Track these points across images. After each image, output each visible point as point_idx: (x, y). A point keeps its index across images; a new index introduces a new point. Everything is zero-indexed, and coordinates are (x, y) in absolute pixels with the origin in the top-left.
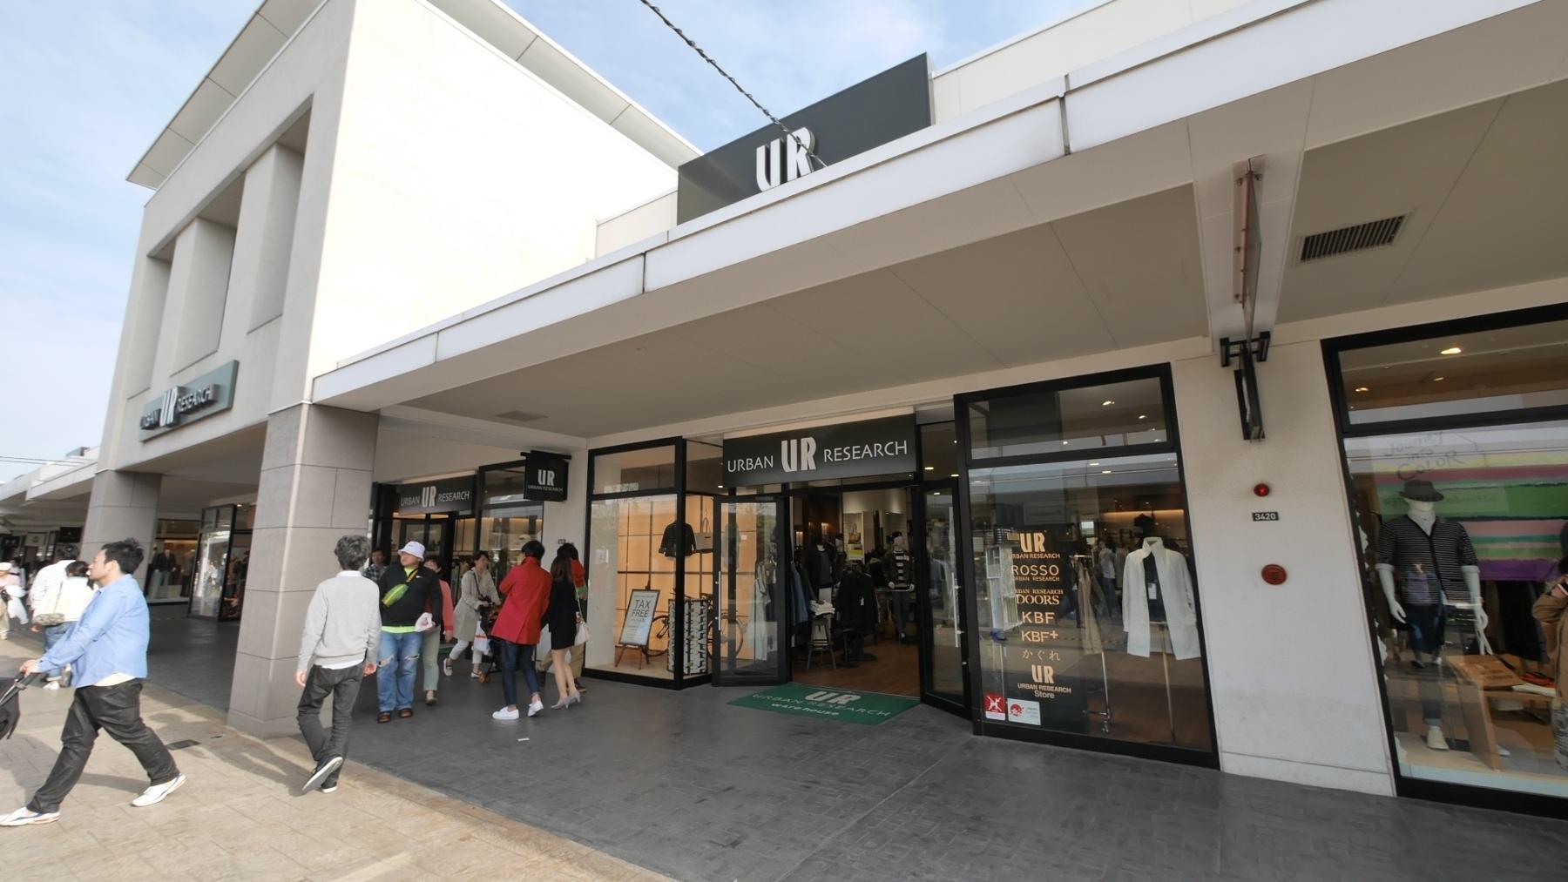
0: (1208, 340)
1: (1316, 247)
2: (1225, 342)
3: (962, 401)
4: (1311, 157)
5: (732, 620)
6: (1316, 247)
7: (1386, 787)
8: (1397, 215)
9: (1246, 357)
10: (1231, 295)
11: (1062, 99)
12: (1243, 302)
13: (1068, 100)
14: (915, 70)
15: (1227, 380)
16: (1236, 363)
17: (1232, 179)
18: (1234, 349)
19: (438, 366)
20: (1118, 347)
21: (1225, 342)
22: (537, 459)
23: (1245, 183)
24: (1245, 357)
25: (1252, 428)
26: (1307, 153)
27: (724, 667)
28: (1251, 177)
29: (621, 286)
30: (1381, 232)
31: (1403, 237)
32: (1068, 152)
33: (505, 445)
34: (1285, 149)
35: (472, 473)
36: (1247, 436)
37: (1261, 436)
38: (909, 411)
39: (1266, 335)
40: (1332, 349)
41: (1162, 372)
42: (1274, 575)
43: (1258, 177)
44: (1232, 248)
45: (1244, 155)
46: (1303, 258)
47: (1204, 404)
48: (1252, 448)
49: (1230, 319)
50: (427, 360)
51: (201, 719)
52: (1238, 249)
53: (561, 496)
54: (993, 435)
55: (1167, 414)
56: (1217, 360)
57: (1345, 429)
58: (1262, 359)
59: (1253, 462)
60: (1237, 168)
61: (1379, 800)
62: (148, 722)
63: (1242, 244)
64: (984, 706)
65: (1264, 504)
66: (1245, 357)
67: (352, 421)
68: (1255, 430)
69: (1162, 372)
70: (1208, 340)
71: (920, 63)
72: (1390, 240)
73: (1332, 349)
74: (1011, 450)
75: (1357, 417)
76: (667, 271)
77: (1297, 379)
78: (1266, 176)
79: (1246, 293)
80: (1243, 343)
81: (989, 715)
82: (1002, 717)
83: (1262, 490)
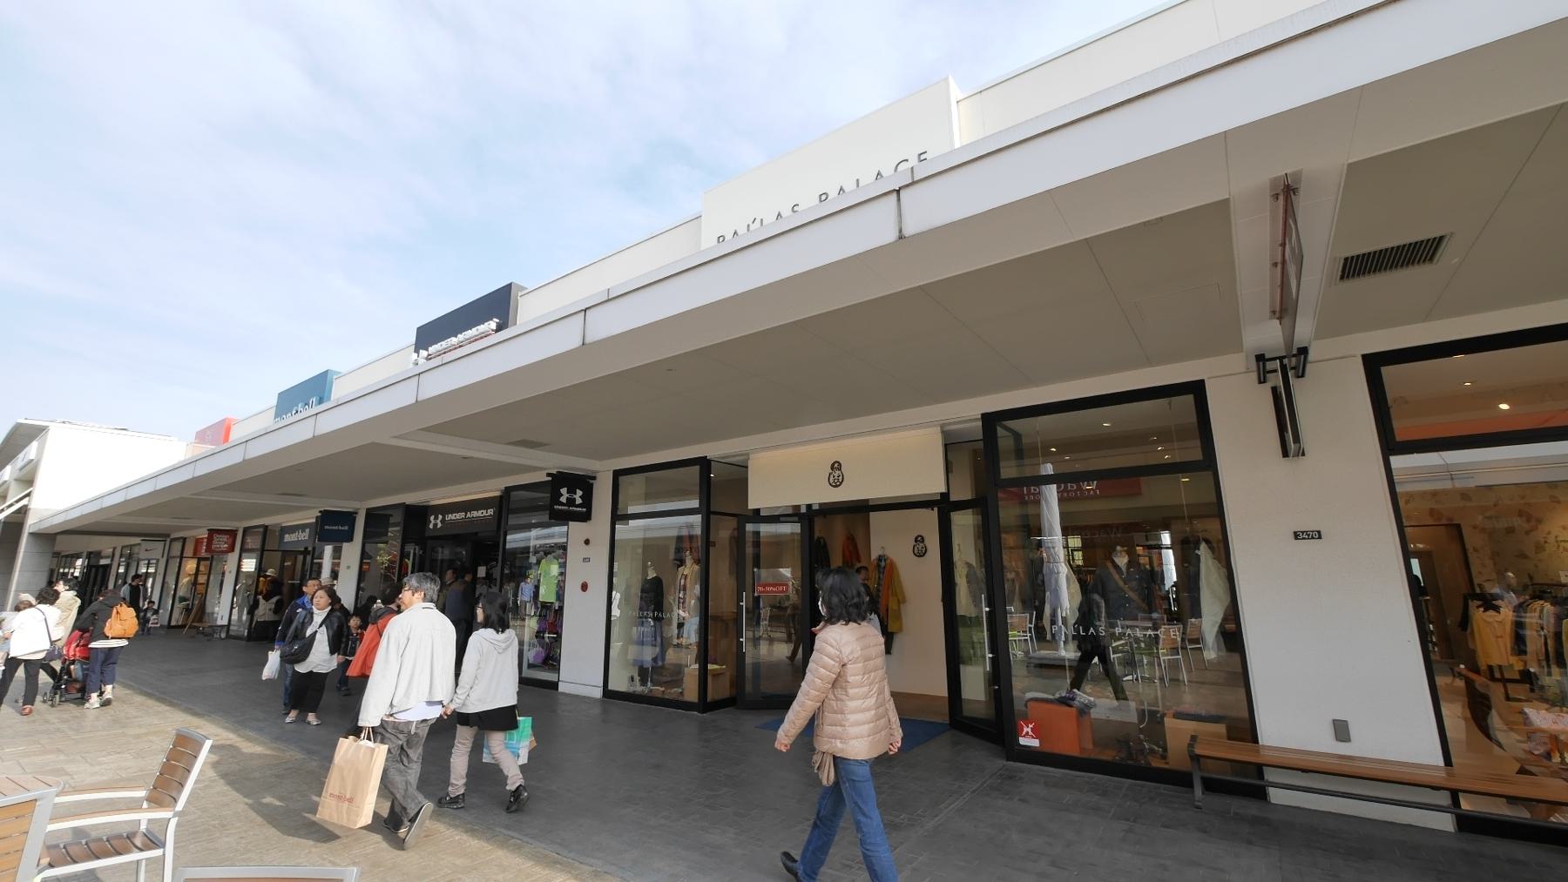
0: (1243, 355)
1: (1355, 267)
2: (1260, 358)
3: (991, 421)
4: (1353, 168)
5: (1053, 622)
6: (1355, 267)
7: (598, 693)
8: (1438, 235)
10: (1268, 314)
12: (1280, 318)
15: (1265, 393)
17: (1268, 199)
20: (1151, 365)
21: (1260, 358)
22: (561, 479)
23: (1281, 198)
24: (1283, 371)
26: (1350, 165)
27: (749, 688)
28: (1287, 192)
30: (1421, 252)
31: (1448, 256)
32: (901, 237)
33: (539, 466)
34: (1320, 164)
35: (498, 494)
36: (1285, 454)
39: (1303, 351)
40: (1374, 364)
41: (1196, 390)
43: (1295, 191)
44: (1268, 265)
45: (1282, 168)
46: (1342, 278)
47: (1238, 417)
49: (1267, 335)
50: (238, 459)
51: (258, 749)
52: (1275, 264)
54: (649, 497)
56: (1254, 376)
57: (1391, 445)
60: (1274, 182)
62: (780, 732)
63: (1279, 259)
64: (1016, 733)
66: (1283, 371)
67: (45, 538)
68: (1292, 446)
69: (1196, 390)
70: (1243, 355)
72: (1431, 259)
73: (1374, 364)
76: (435, 385)
77: (1337, 404)
78: (1302, 192)
79: (1285, 310)
80: (1281, 358)
81: (1023, 741)
82: (1035, 743)
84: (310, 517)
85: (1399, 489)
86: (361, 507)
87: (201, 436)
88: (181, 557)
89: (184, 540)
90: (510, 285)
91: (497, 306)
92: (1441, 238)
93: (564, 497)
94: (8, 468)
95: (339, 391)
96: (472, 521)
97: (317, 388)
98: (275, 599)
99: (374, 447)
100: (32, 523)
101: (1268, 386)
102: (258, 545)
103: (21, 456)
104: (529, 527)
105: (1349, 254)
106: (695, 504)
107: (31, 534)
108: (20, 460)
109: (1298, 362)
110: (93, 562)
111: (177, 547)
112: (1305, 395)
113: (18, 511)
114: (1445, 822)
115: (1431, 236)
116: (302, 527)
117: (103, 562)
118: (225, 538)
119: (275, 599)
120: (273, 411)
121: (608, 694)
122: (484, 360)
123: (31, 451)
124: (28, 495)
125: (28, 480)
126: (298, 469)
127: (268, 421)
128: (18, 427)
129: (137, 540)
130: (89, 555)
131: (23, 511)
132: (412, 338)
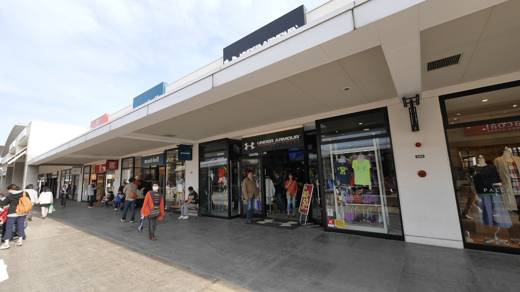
3: (318, 122)
7: (460, 245)
8: (458, 54)
9: (411, 103)
11: (352, 10)
13: (354, 10)
14: (300, 10)
15: (407, 109)
16: (409, 106)
18: (408, 101)
19: (111, 132)
21: (404, 99)
24: (412, 103)
25: (415, 127)
29: (206, 86)
30: (454, 60)
31: (463, 61)
32: (355, 29)
33: (174, 143)
35: (163, 152)
37: (418, 130)
38: (301, 126)
39: (418, 96)
40: (442, 99)
42: (422, 174)
46: (428, 70)
47: (398, 119)
48: (414, 134)
50: (209, 87)
53: (117, 168)
55: (386, 125)
58: (418, 103)
59: (416, 137)
61: (460, 250)
65: (419, 151)
66: (412, 103)
67: (35, 167)
68: (415, 128)
71: (302, 7)
72: (457, 62)
73: (442, 99)
74: (340, 138)
75: (206, 155)
76: (222, 79)
80: (411, 98)
81: (329, 225)
82: (333, 226)
83: (418, 145)
84: (104, 162)
85: (201, 167)
86: (120, 158)
87: (93, 123)
88: (90, 173)
89: (91, 166)
90: (162, 83)
91: (159, 90)
92: (460, 55)
93: (184, 152)
94: (14, 142)
95: (168, 90)
96: (281, 144)
97: (104, 118)
98: (143, 189)
99: (118, 139)
100: (29, 161)
101: (407, 108)
102: (131, 166)
103: (20, 136)
104: (216, 157)
105: (429, 62)
106: (223, 154)
107: (29, 165)
108: (20, 137)
109: (417, 99)
110: (49, 177)
111: (87, 170)
112: (420, 110)
113: (21, 158)
114: (196, 215)
115: (456, 54)
116: (155, 156)
117: (53, 177)
118: (114, 163)
119: (143, 189)
120: (306, 12)
121: (466, 245)
122: (156, 106)
123: (24, 133)
124: (26, 149)
125: (24, 145)
126: (96, 146)
127: (131, 109)
128: (16, 127)
129: (71, 167)
130: (47, 175)
131: (24, 156)
132: (132, 102)
